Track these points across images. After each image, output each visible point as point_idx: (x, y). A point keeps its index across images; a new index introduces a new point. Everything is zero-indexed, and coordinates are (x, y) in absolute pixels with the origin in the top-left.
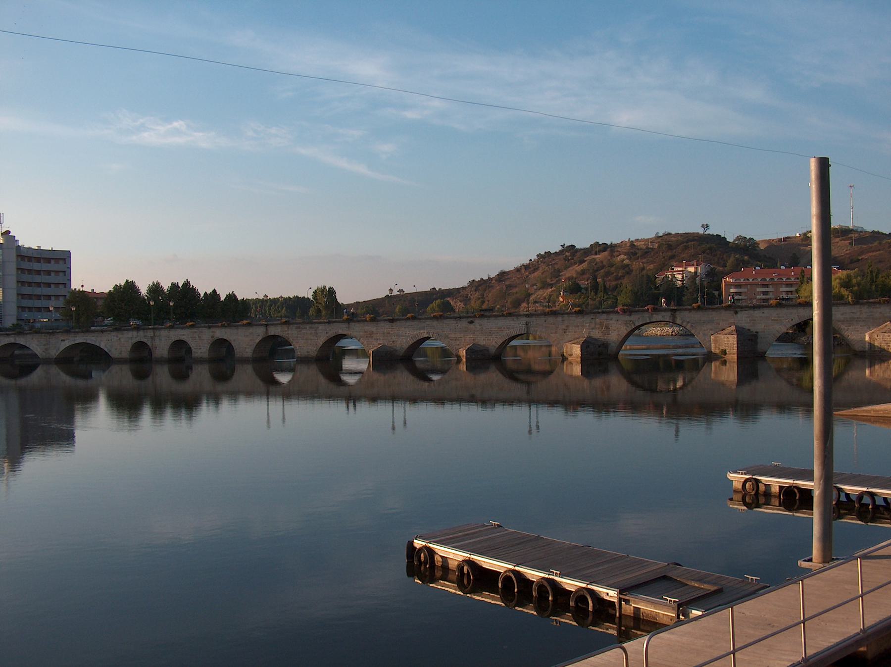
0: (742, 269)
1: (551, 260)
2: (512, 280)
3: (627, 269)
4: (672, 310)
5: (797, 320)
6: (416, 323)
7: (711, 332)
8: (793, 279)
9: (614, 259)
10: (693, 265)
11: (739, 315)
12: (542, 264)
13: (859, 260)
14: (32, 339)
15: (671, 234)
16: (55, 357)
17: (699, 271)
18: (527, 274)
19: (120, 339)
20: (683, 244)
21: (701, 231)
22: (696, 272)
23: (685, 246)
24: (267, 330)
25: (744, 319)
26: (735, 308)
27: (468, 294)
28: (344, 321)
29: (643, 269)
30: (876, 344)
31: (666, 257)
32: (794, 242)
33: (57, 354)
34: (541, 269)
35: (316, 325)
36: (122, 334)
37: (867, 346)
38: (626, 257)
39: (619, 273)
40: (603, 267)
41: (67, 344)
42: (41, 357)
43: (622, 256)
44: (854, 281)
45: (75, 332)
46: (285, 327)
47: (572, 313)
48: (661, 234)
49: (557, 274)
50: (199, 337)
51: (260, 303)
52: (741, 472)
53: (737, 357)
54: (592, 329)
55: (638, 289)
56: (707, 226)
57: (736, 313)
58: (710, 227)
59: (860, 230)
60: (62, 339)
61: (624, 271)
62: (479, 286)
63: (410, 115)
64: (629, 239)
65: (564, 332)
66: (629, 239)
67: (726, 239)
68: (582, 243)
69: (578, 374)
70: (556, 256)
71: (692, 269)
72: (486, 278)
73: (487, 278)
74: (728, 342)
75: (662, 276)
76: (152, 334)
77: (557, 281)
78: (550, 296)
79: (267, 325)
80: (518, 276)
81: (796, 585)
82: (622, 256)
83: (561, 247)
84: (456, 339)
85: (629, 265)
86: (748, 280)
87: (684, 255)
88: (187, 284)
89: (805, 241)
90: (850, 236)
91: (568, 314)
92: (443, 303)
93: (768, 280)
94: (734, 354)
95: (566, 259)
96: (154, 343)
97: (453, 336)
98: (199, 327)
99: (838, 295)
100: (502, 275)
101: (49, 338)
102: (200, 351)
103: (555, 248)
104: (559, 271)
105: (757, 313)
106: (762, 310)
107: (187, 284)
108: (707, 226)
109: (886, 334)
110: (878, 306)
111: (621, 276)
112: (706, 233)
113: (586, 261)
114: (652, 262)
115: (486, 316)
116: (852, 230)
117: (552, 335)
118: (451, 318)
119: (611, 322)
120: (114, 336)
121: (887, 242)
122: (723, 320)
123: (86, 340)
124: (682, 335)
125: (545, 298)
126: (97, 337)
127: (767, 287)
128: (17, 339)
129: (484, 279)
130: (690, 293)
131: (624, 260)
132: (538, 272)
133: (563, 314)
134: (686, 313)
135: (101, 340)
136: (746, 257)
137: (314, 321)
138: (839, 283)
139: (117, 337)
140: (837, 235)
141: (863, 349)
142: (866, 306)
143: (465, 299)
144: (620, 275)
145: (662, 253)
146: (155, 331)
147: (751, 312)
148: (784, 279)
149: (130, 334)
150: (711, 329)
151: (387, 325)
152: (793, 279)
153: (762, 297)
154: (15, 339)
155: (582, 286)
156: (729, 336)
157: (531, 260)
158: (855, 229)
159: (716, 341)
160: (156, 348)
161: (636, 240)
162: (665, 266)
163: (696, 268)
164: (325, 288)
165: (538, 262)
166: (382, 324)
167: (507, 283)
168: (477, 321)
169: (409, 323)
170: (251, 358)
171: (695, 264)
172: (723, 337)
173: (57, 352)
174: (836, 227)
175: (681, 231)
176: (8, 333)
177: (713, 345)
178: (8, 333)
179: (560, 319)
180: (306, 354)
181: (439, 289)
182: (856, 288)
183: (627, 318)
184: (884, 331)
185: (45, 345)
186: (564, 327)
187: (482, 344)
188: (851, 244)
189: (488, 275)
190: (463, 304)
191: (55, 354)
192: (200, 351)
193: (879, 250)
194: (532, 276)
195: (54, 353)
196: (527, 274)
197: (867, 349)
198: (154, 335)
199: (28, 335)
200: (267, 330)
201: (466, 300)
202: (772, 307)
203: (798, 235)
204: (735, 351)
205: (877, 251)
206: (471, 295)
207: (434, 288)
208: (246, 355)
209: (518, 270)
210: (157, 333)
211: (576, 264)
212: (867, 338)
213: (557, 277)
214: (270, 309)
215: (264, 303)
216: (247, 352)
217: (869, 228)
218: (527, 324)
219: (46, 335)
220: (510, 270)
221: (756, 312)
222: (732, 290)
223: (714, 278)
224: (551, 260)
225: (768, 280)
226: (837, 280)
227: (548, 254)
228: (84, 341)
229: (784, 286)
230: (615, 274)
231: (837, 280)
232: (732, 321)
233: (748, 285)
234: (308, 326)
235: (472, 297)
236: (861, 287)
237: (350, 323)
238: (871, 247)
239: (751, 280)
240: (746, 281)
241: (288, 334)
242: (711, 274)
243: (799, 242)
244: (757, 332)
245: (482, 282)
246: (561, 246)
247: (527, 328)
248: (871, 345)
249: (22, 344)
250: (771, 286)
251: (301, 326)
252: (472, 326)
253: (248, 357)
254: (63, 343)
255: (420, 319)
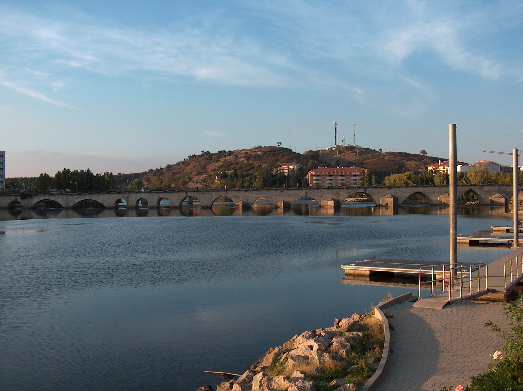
0: (318, 168)
1: (197, 159)
2: (175, 170)
3: (251, 166)
4: (365, 188)
5: (117, 199)
6: (257, 192)
7: (380, 197)
8: (344, 173)
9: (238, 160)
10: (292, 165)
11: (391, 190)
12: (192, 161)
13: (363, 164)
14: (59, 197)
15: (262, 147)
16: (72, 206)
17: (295, 168)
18: (184, 166)
19: (109, 198)
20: (282, 153)
21: (277, 146)
22: (293, 169)
23: (283, 155)
24: (187, 194)
25: (392, 191)
26: (389, 188)
27: (149, 177)
28: (225, 191)
29: (261, 166)
30: (443, 201)
31: (273, 160)
32: (325, 153)
33: (73, 205)
34: (192, 164)
35: (211, 192)
36: (111, 195)
37: (438, 202)
38: (245, 159)
39: (247, 168)
40: (232, 164)
41: (79, 200)
42: (63, 206)
43: (243, 159)
44: (412, 177)
45: (84, 194)
46: (196, 193)
47: (324, 189)
48: (256, 147)
49: (204, 167)
50: (152, 197)
51: (24, 180)
52: (352, 265)
53: (394, 207)
54: (333, 195)
55: (266, 177)
56: (280, 143)
57: (390, 189)
58: (282, 144)
59: (359, 147)
60: (77, 197)
61: (250, 167)
62: (155, 173)
63: (74, 64)
64: (238, 149)
65: (322, 196)
66: (238, 149)
67: (292, 150)
68: (214, 150)
69: (502, 202)
70: (200, 157)
71: (291, 167)
72: (159, 168)
73: (160, 168)
74: (390, 201)
75: (276, 170)
76: (127, 196)
77: (205, 171)
78: (205, 179)
79: (16, 196)
80: (179, 168)
81: (418, 301)
82: (243, 159)
83: (202, 152)
84: (275, 199)
85: (252, 164)
86: (322, 173)
87: (283, 160)
88: (89, 170)
89: (331, 152)
90: (355, 150)
91: (323, 189)
92: (138, 181)
93: (331, 173)
94: (392, 205)
95: (206, 159)
96: (128, 200)
97: (274, 197)
98: (152, 193)
99: (406, 182)
100: (169, 167)
101: (69, 197)
102: (152, 203)
103: (199, 153)
104: (205, 166)
105: (398, 189)
106: (399, 188)
107: (89, 170)
108: (280, 143)
109: (447, 198)
110: (442, 187)
111: (248, 169)
112: (280, 147)
113: (220, 160)
114: (265, 163)
115: (288, 189)
116: (355, 147)
117: (316, 197)
118: (273, 190)
119: (341, 192)
120: (106, 196)
121: (376, 155)
122: (385, 192)
123: (91, 198)
124: (300, 200)
125: (202, 180)
126: (97, 196)
127: (331, 177)
128: (49, 197)
129: (158, 169)
130: (293, 179)
131: (244, 161)
132: (190, 166)
133: (320, 189)
134: (370, 189)
135: (99, 198)
136: (316, 161)
137: (260, 189)
138: (407, 177)
139: (108, 197)
140: (348, 149)
141: (437, 204)
142: (438, 187)
143: (148, 180)
144: (248, 168)
145: (270, 158)
146: (129, 194)
147: (395, 189)
148: (339, 173)
149: (115, 195)
150: (380, 196)
151: (245, 192)
152: (344, 173)
153: (329, 182)
154: (48, 197)
155: (228, 174)
156: (389, 198)
157: (185, 159)
158: (357, 146)
159: (382, 200)
160: (129, 202)
161: (243, 149)
162: (273, 165)
163: (294, 167)
164: (108, 173)
165: (189, 160)
166: (242, 192)
167: (173, 171)
168: (285, 191)
169: (255, 192)
170: (178, 207)
171: (293, 164)
172: (386, 198)
173: (73, 204)
174: (347, 145)
175: (267, 145)
176: (44, 194)
177: (381, 202)
178: (44, 194)
179: (319, 191)
180: (206, 205)
181: (123, 174)
182: (413, 180)
183: (347, 191)
184: (445, 196)
185: (66, 200)
186: (321, 194)
187: (287, 201)
188: (356, 155)
189: (161, 167)
190: (147, 183)
191: (72, 205)
192: (152, 203)
193: (373, 158)
194: (187, 168)
195: (71, 204)
196: (184, 166)
197: (438, 204)
198: (128, 196)
199: (56, 196)
200: (187, 194)
201: (149, 181)
202: (404, 187)
203: (327, 149)
204: (393, 204)
205: (372, 159)
206: (151, 178)
207: (120, 173)
208: (176, 205)
209: (178, 164)
210: (130, 195)
211: (214, 162)
212: (438, 199)
213: (205, 169)
214: (30, 184)
215: (27, 180)
216: (177, 204)
217: (364, 146)
218: (306, 193)
219: (67, 195)
220: (173, 164)
221: (397, 189)
222: (314, 178)
223: (303, 172)
224: (197, 159)
225: (331, 173)
226: (406, 176)
227: (194, 156)
228: (89, 199)
229: (339, 176)
230: (244, 168)
231: (406, 176)
232: (388, 192)
233: (322, 175)
234: (207, 193)
235: (151, 179)
236: (415, 179)
237: (227, 192)
238: (368, 157)
239: (323, 173)
240: (321, 174)
241: (197, 196)
242: (300, 170)
243: (328, 153)
244: (397, 197)
245: (157, 171)
246: (202, 152)
247: (306, 194)
248: (440, 202)
249: (80, 201)
250: (333, 176)
251: (204, 192)
252: (282, 193)
253: (178, 206)
254: (77, 199)
255: (259, 190)
